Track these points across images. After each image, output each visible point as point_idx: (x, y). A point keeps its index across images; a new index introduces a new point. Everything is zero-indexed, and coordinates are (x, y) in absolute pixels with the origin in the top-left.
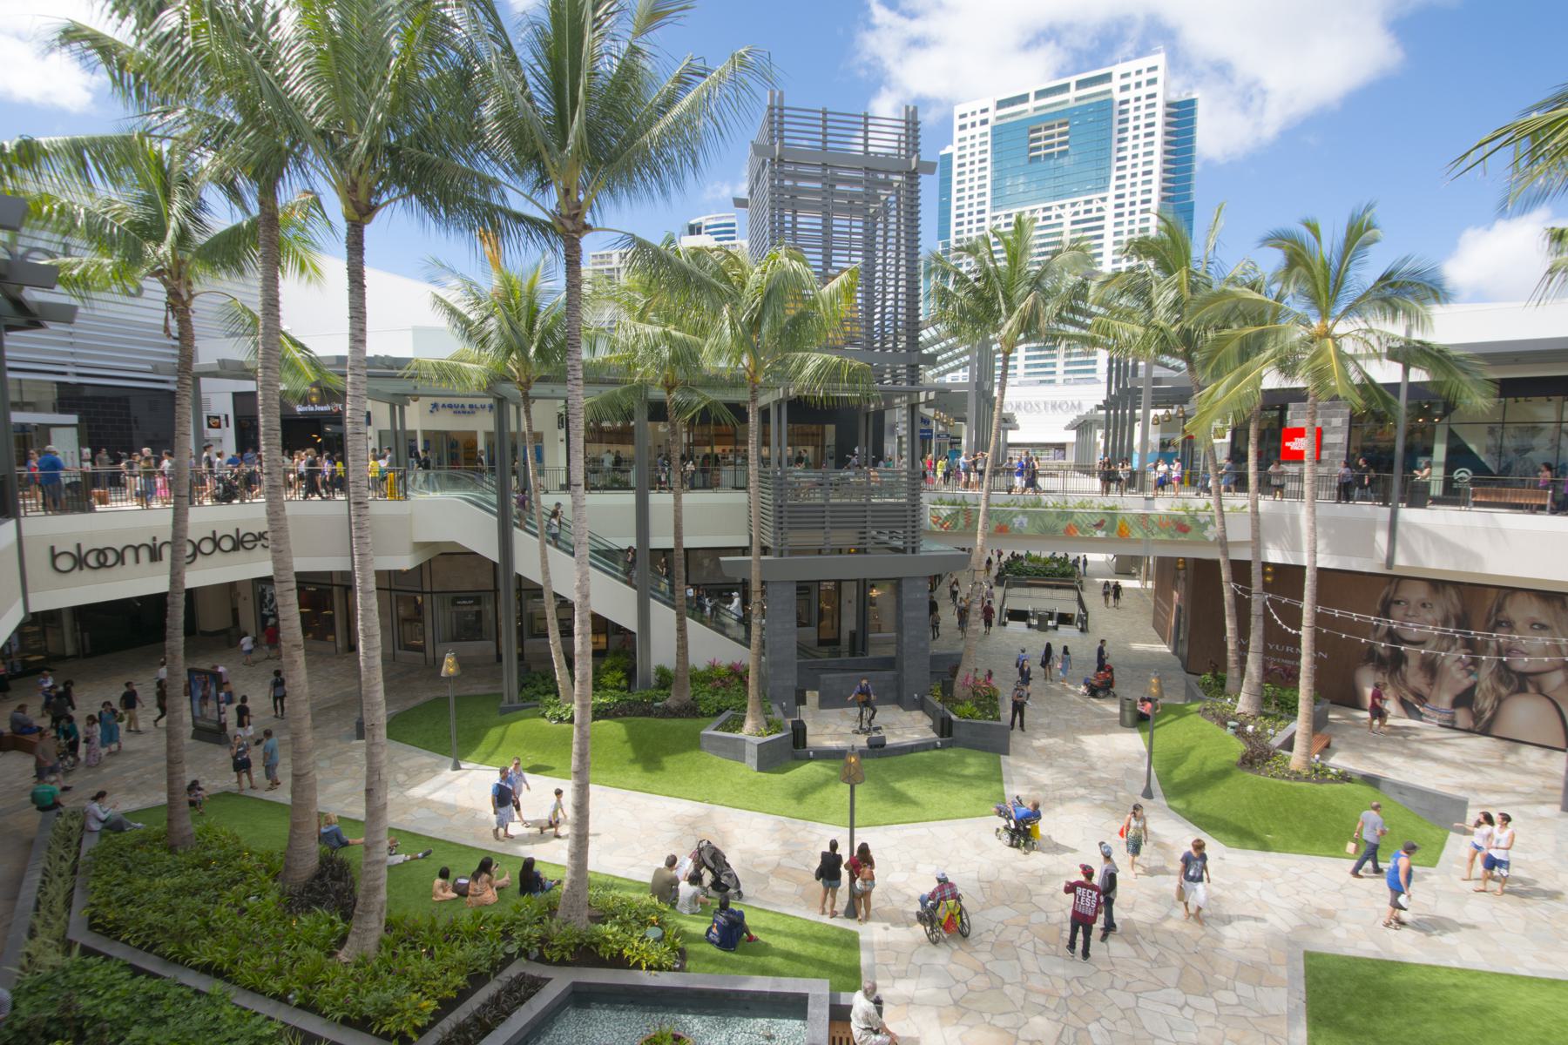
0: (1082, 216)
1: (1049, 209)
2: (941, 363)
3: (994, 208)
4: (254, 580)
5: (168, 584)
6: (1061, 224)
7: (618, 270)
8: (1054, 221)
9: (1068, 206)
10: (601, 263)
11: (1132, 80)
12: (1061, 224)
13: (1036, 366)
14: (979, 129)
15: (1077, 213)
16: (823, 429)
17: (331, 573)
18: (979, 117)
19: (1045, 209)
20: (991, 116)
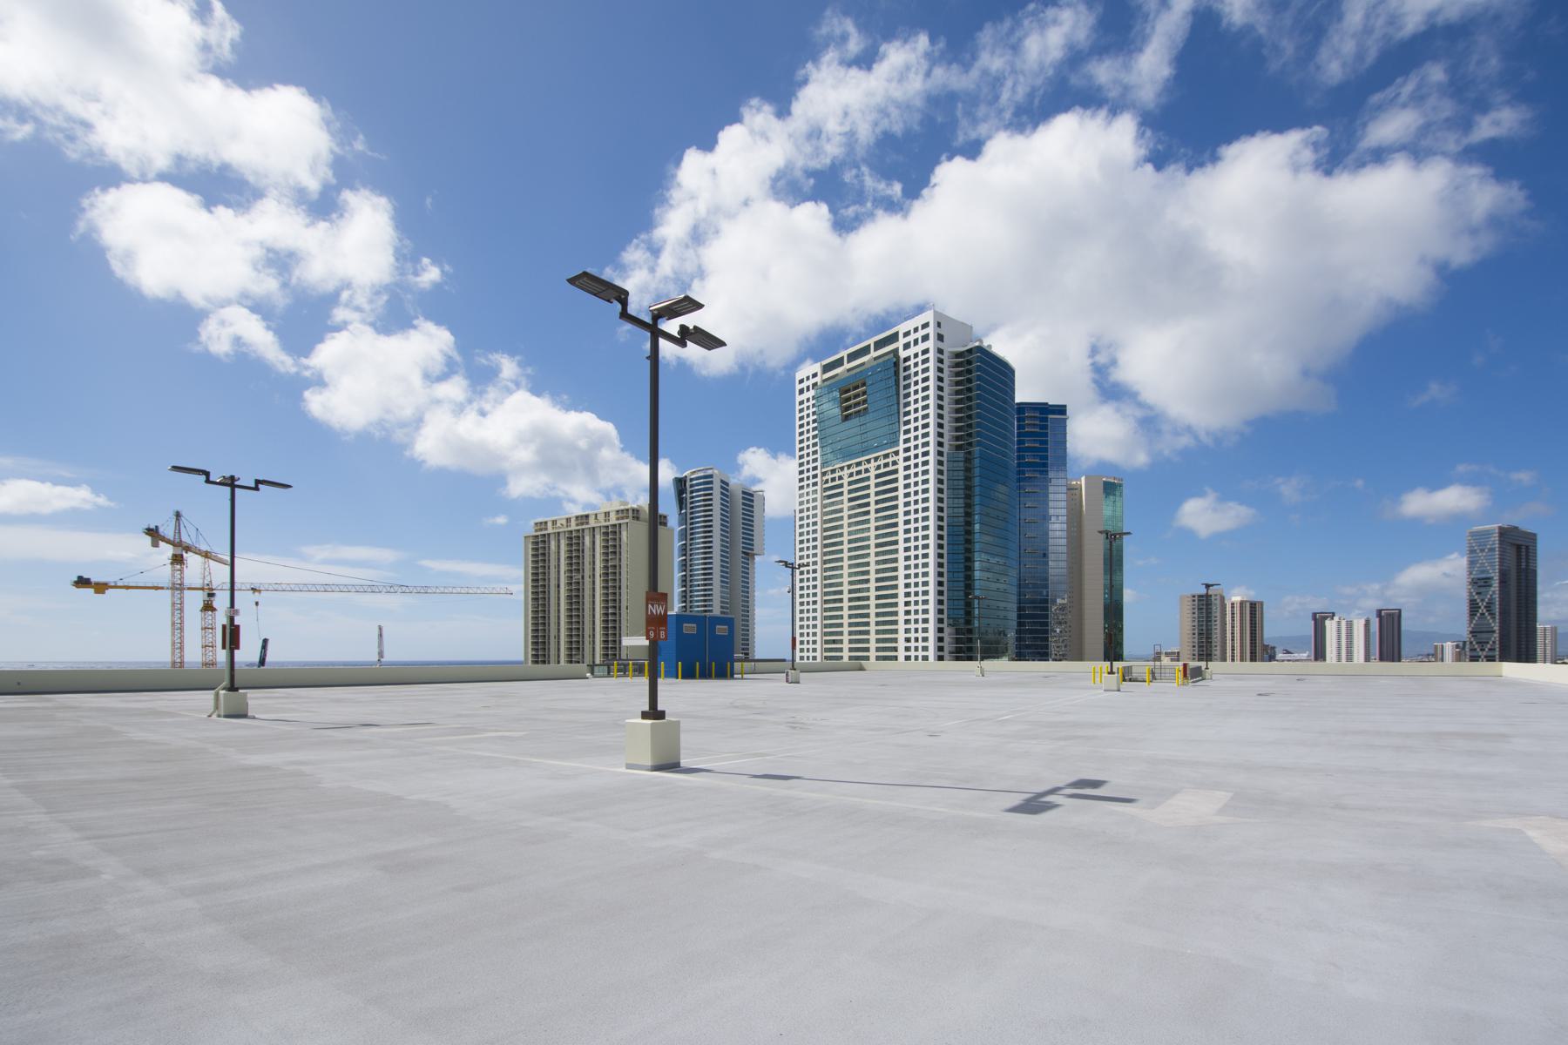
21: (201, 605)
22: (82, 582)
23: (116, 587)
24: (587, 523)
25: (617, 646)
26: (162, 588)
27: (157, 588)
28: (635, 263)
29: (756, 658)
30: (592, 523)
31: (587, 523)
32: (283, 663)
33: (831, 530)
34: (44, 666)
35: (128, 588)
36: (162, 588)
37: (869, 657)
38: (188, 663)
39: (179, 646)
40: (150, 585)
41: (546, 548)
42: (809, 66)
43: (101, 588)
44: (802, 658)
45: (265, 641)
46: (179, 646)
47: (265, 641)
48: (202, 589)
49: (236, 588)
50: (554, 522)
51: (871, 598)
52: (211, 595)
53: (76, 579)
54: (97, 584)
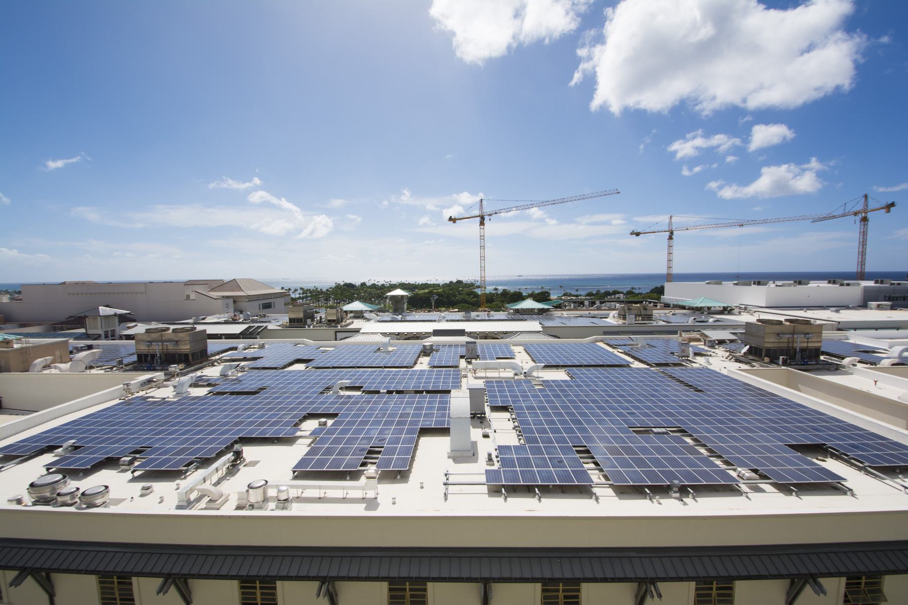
27: (654, 232)
36: (655, 232)
48: (669, 231)
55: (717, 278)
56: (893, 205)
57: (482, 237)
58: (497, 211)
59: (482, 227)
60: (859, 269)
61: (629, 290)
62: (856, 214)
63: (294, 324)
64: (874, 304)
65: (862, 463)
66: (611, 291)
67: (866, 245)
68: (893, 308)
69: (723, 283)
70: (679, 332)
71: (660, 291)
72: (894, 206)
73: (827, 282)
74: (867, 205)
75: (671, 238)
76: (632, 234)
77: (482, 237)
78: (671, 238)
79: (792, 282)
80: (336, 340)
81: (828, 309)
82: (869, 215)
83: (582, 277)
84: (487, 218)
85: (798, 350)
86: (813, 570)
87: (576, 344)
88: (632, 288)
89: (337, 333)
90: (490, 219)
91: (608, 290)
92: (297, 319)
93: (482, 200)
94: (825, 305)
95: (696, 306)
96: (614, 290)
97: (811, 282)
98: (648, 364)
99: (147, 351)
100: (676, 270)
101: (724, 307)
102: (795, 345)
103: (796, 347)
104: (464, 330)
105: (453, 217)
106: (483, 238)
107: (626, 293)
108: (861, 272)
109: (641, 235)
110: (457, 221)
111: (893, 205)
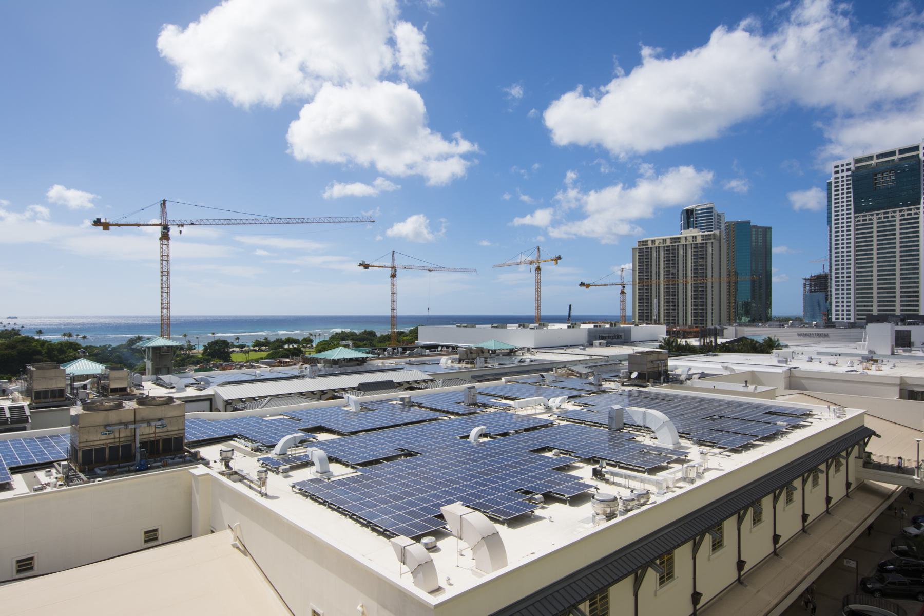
0: (906, 217)
1: (865, 216)
2: (260, 364)
3: (855, 212)
4: (916, 400)
5: (152, 396)
6: (872, 224)
7: (651, 248)
8: (913, 216)
9: (898, 212)
10: (643, 245)
11: (840, 169)
12: (872, 224)
13: (883, 293)
14: (846, 174)
15: (880, 218)
16: (855, 320)
17: (909, 399)
18: (845, 168)
19: (885, 213)
20: (852, 167)
21: (620, 291)
22: (582, 284)
23: (592, 286)
24: (679, 242)
25: (650, 301)
26: (607, 285)
27: (605, 285)
28: (474, 145)
29: (568, 315)
30: (683, 242)
31: (679, 242)
32: (279, 316)
33: (885, 263)
34: (94, 320)
35: (596, 286)
36: (607, 285)
37: (895, 260)
38: (173, 317)
39: (623, 309)
40: (603, 284)
41: (676, 256)
42: (552, 142)
43: (588, 286)
44: (837, 319)
45: (570, 306)
46: (623, 309)
47: (570, 306)
48: (621, 285)
49: (631, 286)
50: (653, 241)
51: (874, 250)
52: (624, 287)
53: (580, 283)
54: (587, 285)
55: (501, 322)
56: (559, 258)
57: (165, 258)
58: (195, 222)
59: (165, 242)
60: (537, 314)
61: (306, 337)
62: (531, 263)
63: (46, 401)
64: (597, 342)
65: (644, 468)
66: (284, 339)
67: (540, 291)
68: (607, 345)
69: (477, 326)
70: (554, 369)
71: (414, 334)
72: (560, 259)
73: (517, 325)
74: (539, 256)
75: (394, 276)
76: (361, 265)
77: (165, 258)
78: (394, 276)
79: (537, 325)
80: (211, 411)
81: (578, 348)
82: (542, 266)
83: (231, 318)
84: (173, 231)
85: (662, 372)
86: (573, 602)
87: (236, 419)
88: (311, 335)
89: (208, 403)
90: (181, 232)
91: (280, 338)
92: (52, 391)
93: (164, 201)
94: (569, 344)
95: (332, 358)
96: (287, 337)
97: (550, 324)
98: (339, 433)
99: (153, 435)
100: (544, 312)
101: (510, 349)
102: (660, 369)
103: (661, 370)
104: (391, 382)
105: (103, 221)
106: (165, 258)
107: (303, 340)
108: (538, 316)
109: (590, 288)
110: (111, 228)
111: (559, 258)
